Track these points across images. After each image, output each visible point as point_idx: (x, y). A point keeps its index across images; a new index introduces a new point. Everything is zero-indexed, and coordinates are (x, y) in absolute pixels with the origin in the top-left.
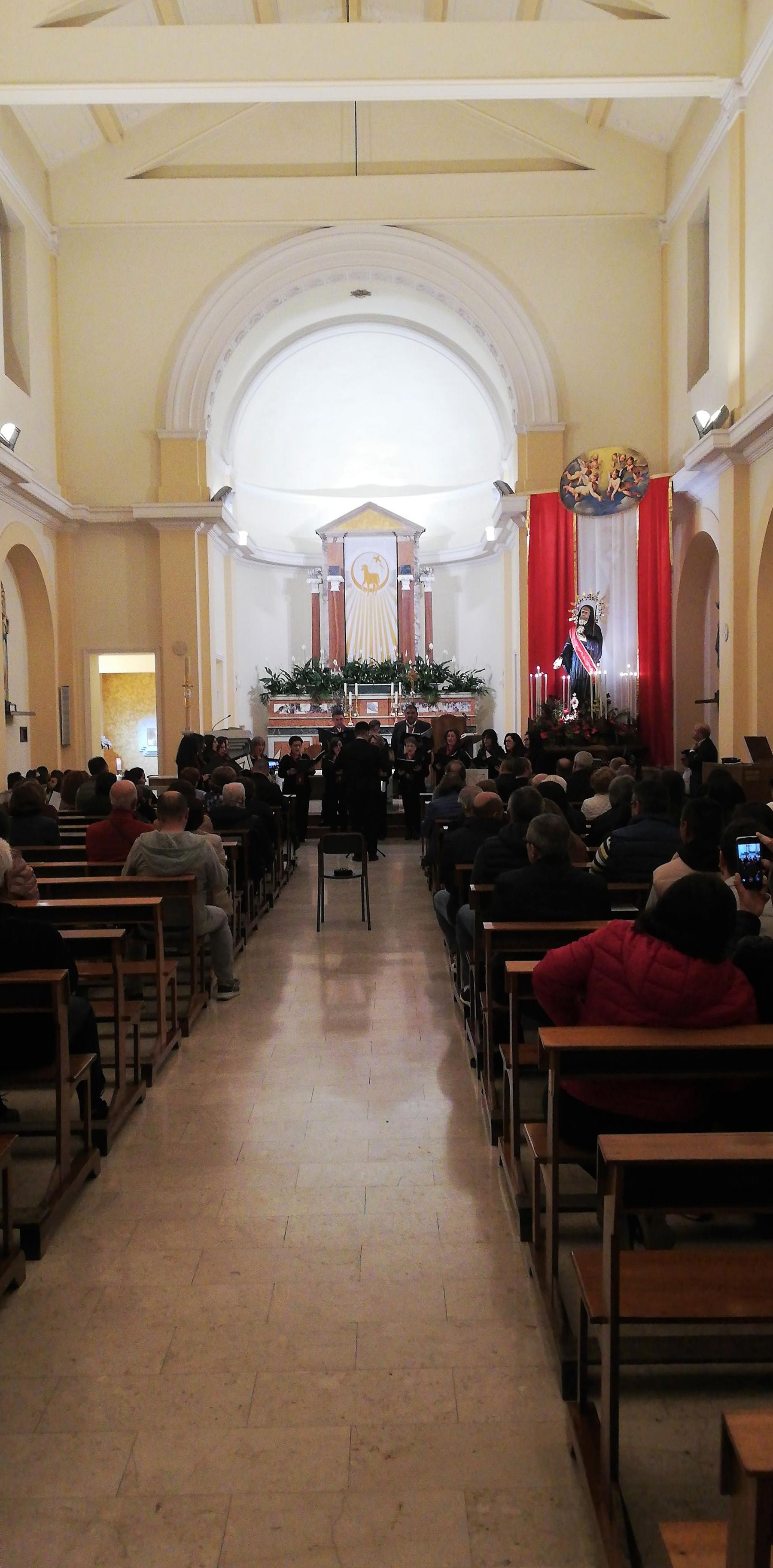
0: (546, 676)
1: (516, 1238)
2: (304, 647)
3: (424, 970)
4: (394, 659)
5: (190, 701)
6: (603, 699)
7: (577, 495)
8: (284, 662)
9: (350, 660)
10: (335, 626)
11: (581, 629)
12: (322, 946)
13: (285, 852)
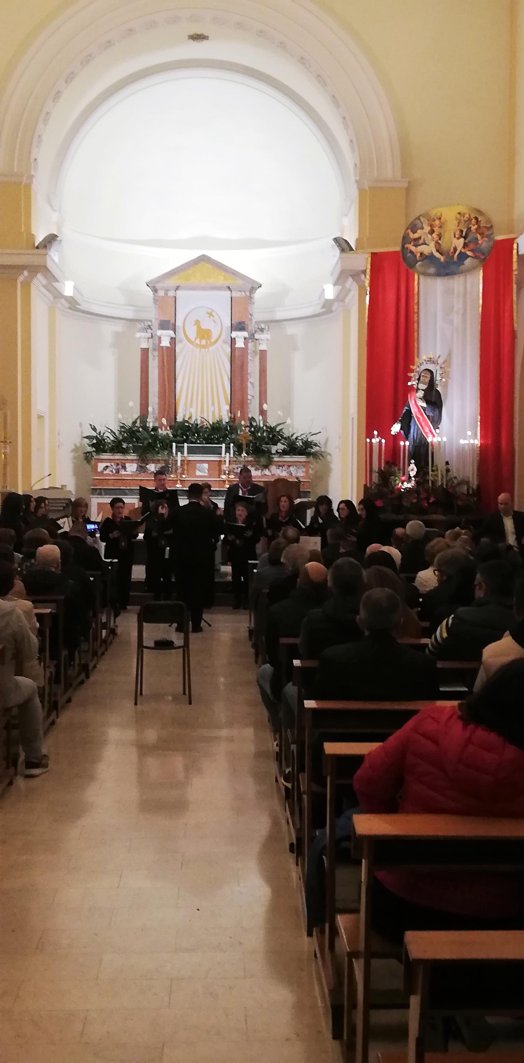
0: (383, 441)
1: (328, 1034)
2: (131, 404)
3: (251, 748)
4: (226, 419)
5: (8, 457)
6: (441, 466)
7: (418, 255)
8: (110, 419)
9: (180, 419)
10: (164, 381)
11: (421, 394)
12: (140, 721)
13: (104, 620)
